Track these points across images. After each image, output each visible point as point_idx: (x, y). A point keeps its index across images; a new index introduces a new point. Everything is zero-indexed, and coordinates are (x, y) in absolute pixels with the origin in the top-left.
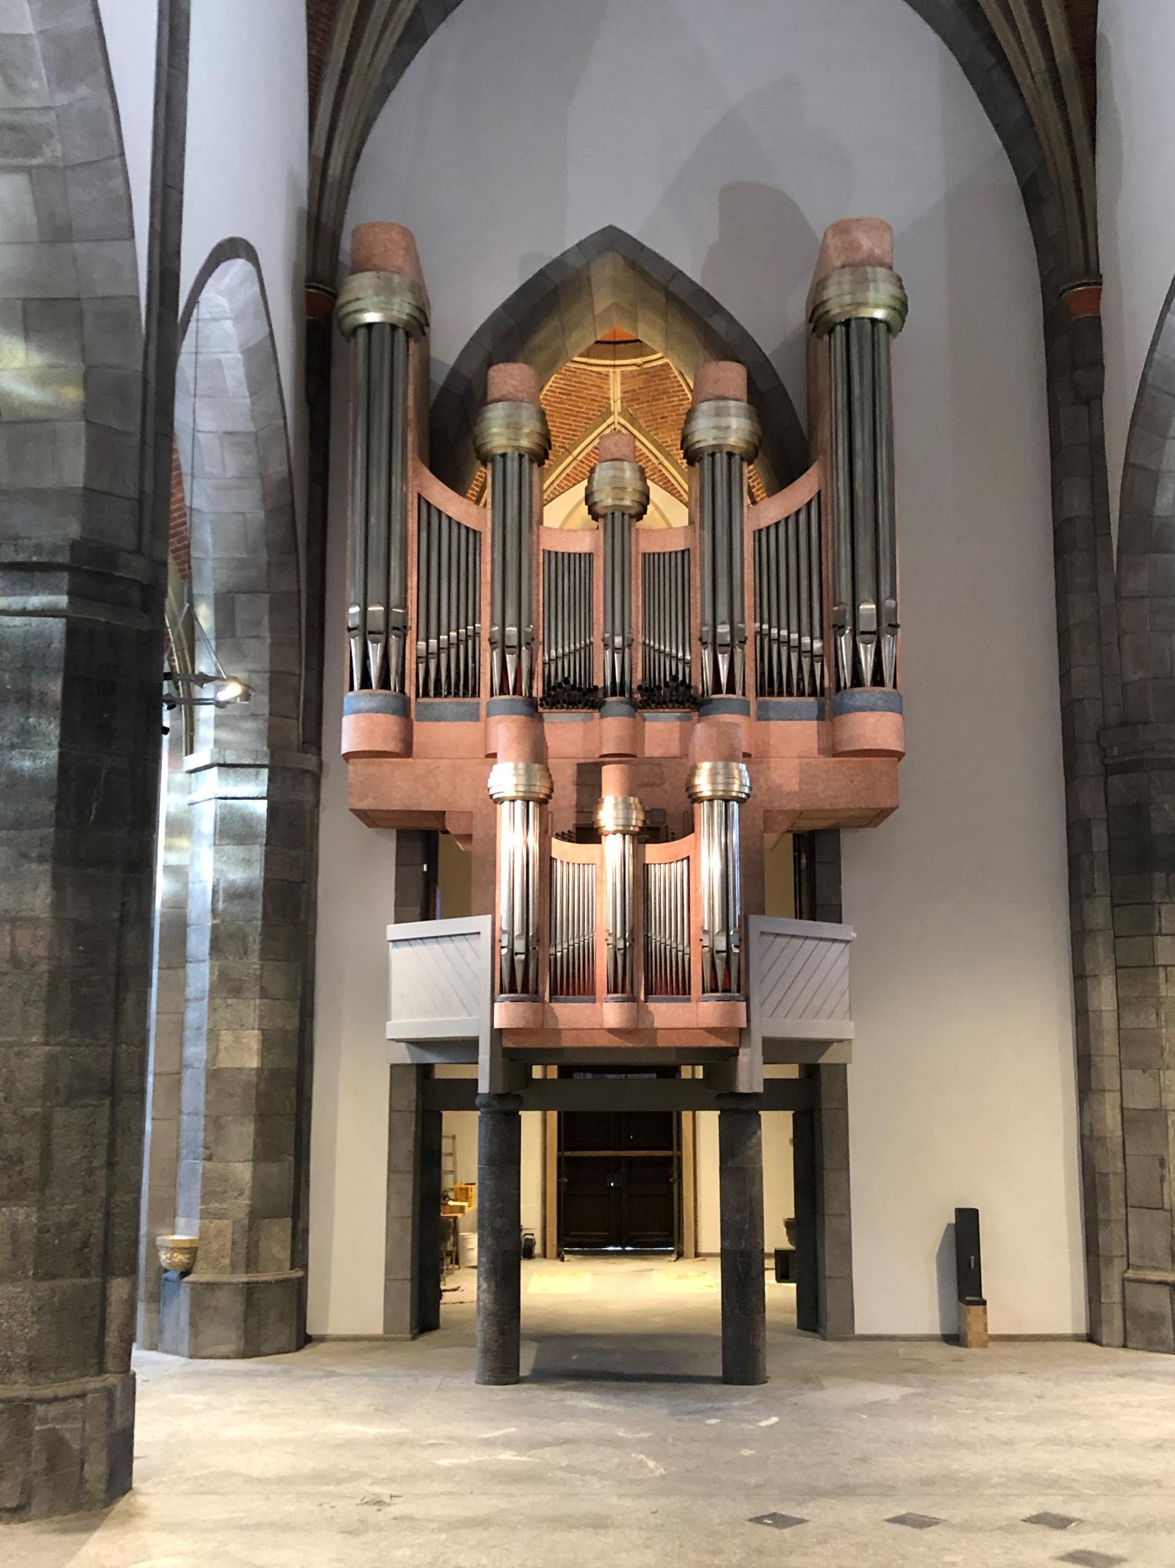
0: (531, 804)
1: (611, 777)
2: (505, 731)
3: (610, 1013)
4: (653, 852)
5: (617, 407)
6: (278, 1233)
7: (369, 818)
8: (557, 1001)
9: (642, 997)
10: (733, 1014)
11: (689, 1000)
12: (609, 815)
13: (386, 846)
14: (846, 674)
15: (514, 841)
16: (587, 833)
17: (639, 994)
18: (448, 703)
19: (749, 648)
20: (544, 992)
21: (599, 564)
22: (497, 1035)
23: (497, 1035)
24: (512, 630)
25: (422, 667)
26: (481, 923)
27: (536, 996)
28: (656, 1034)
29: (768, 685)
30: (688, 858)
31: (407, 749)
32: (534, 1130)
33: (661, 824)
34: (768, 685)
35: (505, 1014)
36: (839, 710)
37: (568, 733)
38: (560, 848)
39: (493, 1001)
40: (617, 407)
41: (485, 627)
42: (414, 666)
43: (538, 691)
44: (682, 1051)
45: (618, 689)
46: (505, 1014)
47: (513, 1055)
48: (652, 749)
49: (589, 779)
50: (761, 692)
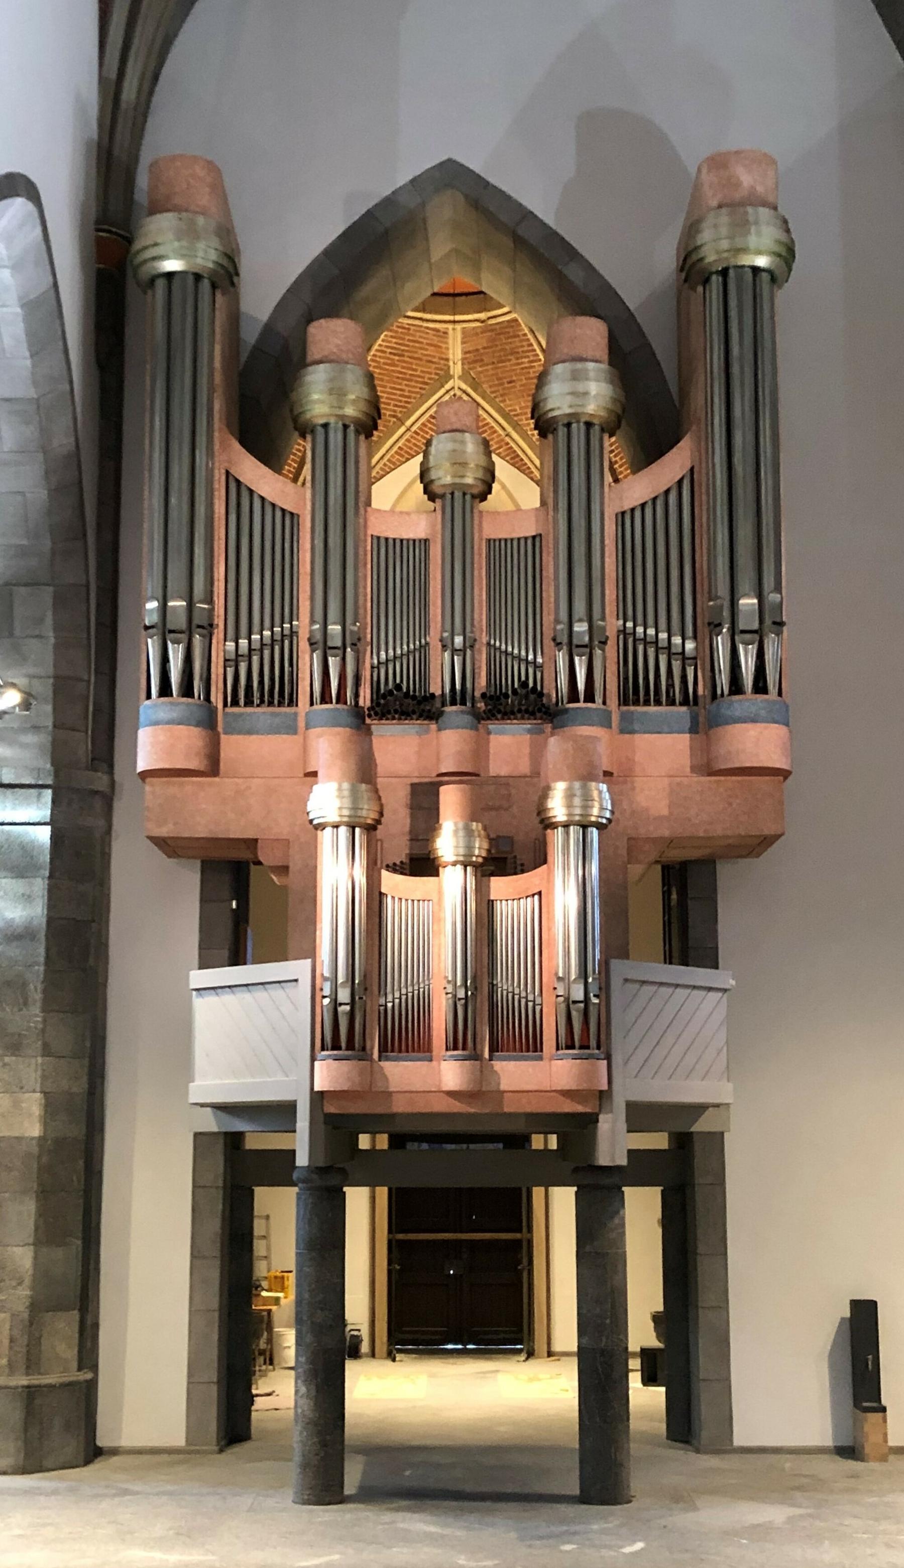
0: (357, 830)
1: (451, 799)
2: (327, 746)
3: (450, 1073)
4: (499, 886)
5: (457, 369)
6: (62, 1332)
7: (170, 847)
8: (388, 1059)
9: (486, 1055)
10: (591, 1075)
11: (541, 1058)
12: (447, 843)
13: (189, 880)
14: (723, 680)
15: (338, 873)
16: (423, 864)
17: (482, 1051)
18: (260, 713)
19: (611, 649)
20: (372, 1048)
21: (436, 552)
22: (318, 1098)
23: (318, 1098)
24: (335, 629)
25: (230, 671)
26: (299, 968)
27: (363, 1054)
28: (502, 1097)
29: (632, 694)
30: (540, 893)
31: (213, 767)
32: (359, 1204)
33: (509, 854)
34: (632, 694)
35: (328, 1074)
36: (715, 722)
37: (401, 748)
38: (390, 882)
39: (313, 1059)
40: (457, 369)
41: (304, 625)
42: (221, 671)
43: (365, 699)
44: (533, 1118)
45: (459, 697)
46: (328, 1074)
47: (337, 1123)
48: (497, 767)
49: (424, 800)
50: (624, 700)
